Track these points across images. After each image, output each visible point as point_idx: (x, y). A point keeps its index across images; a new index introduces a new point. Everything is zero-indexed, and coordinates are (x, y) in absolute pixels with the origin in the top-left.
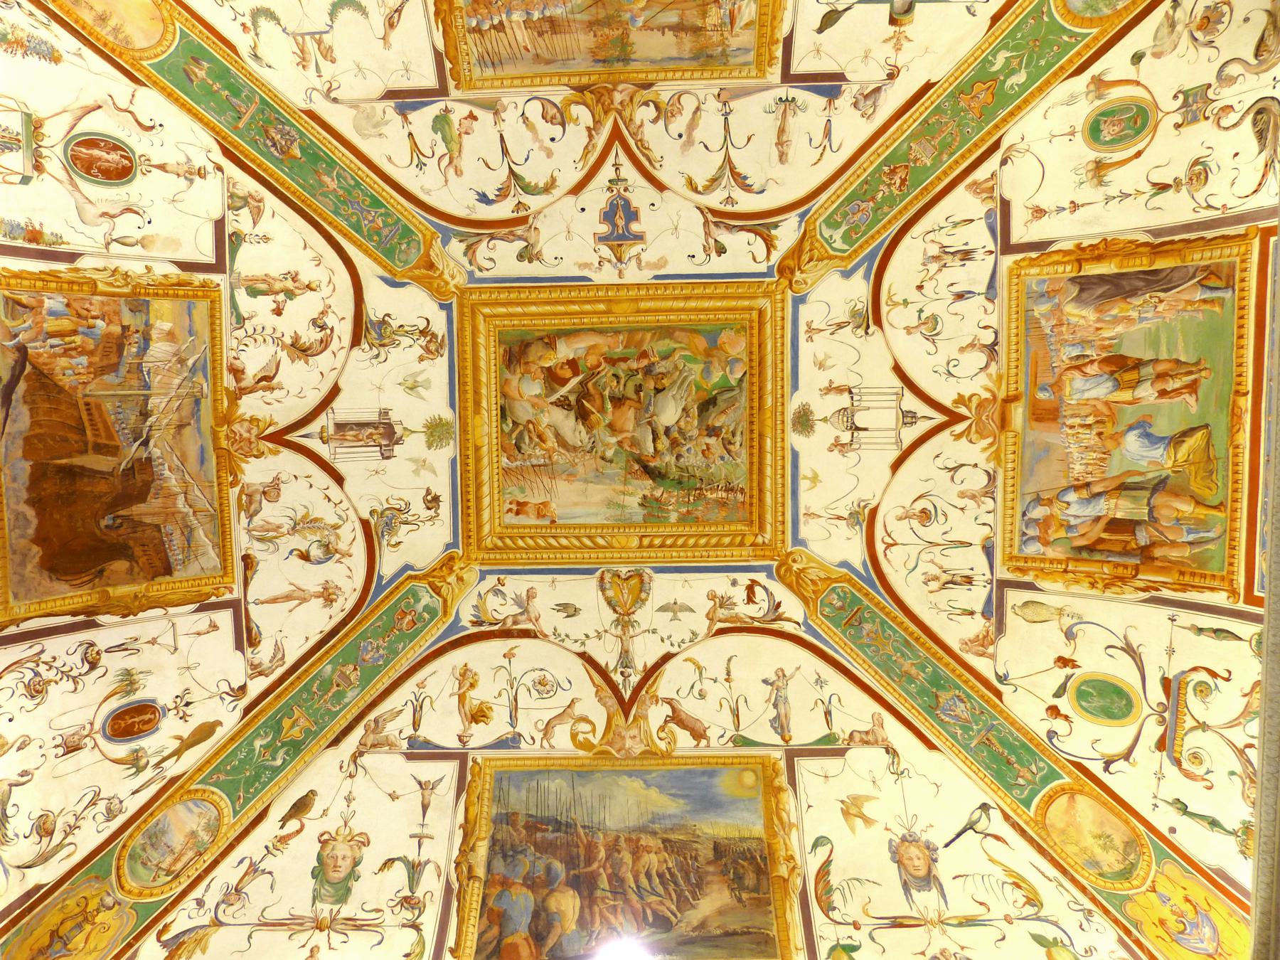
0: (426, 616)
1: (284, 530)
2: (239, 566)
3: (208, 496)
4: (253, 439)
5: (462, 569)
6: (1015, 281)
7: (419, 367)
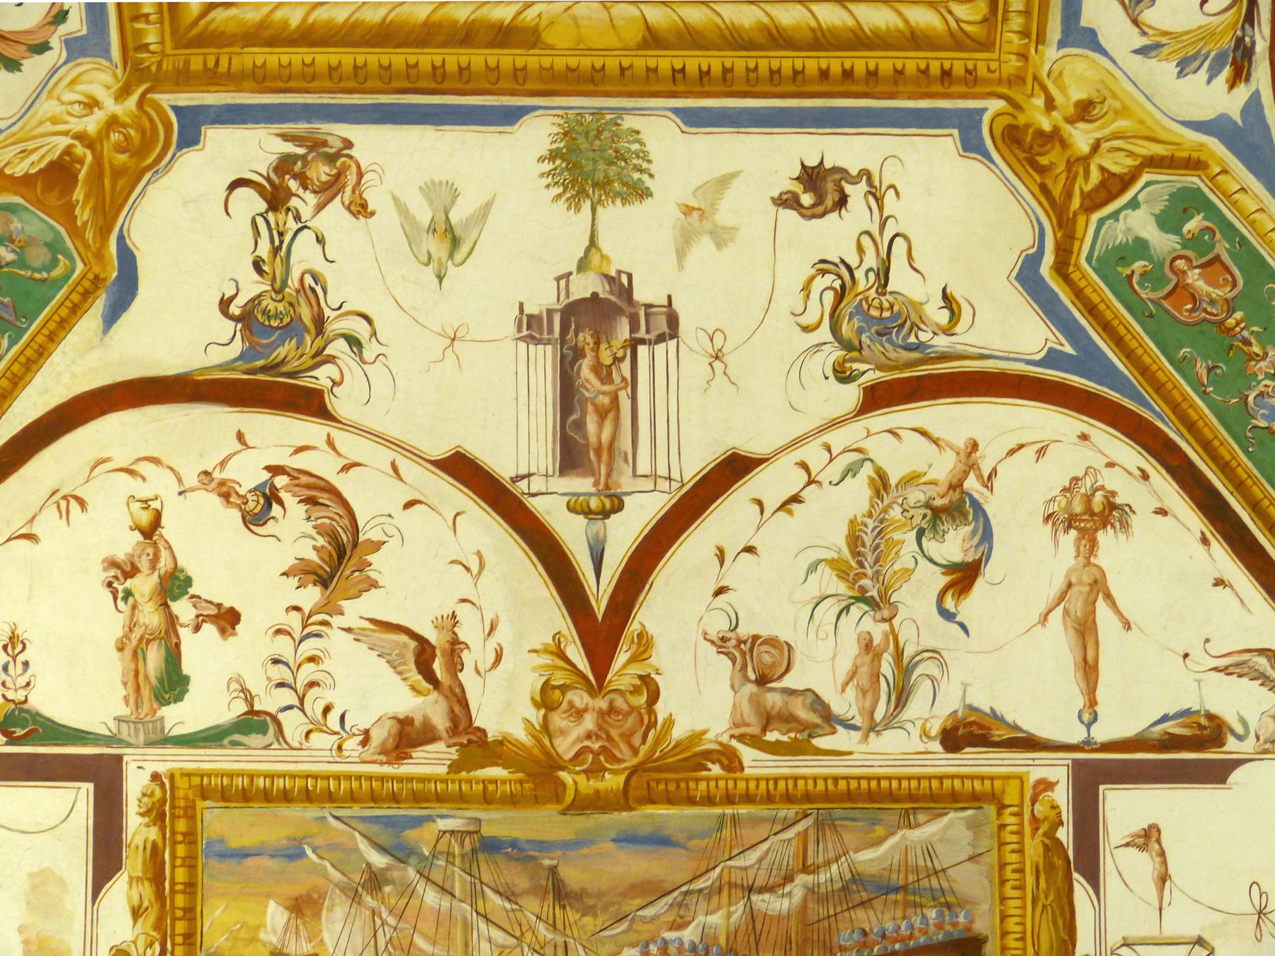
0: (1193, 225)
1: (878, 631)
2: (973, 761)
3: (763, 831)
4: (603, 704)
5: (1050, 105)
7: (386, 219)
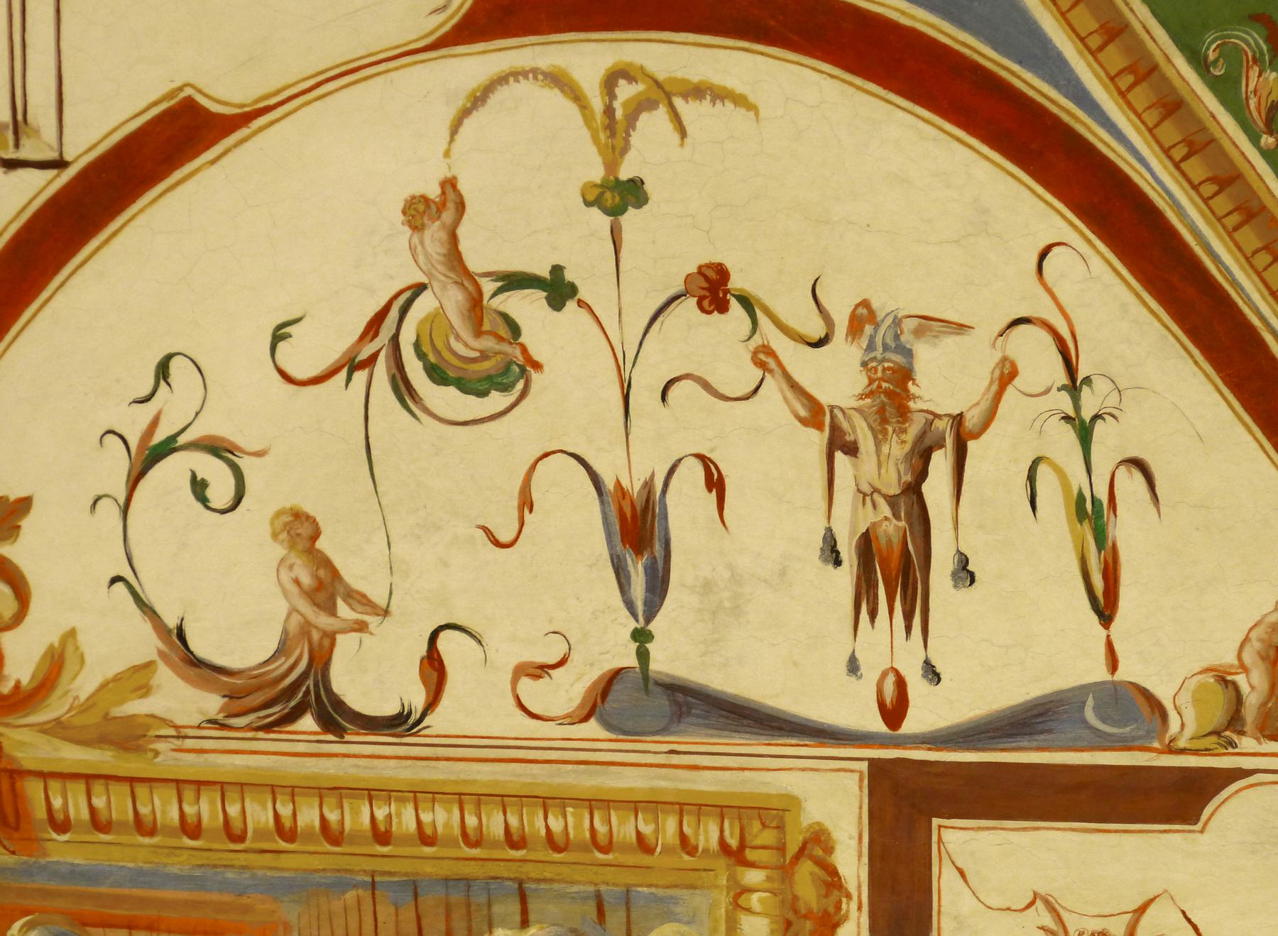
6: (708, 835)
